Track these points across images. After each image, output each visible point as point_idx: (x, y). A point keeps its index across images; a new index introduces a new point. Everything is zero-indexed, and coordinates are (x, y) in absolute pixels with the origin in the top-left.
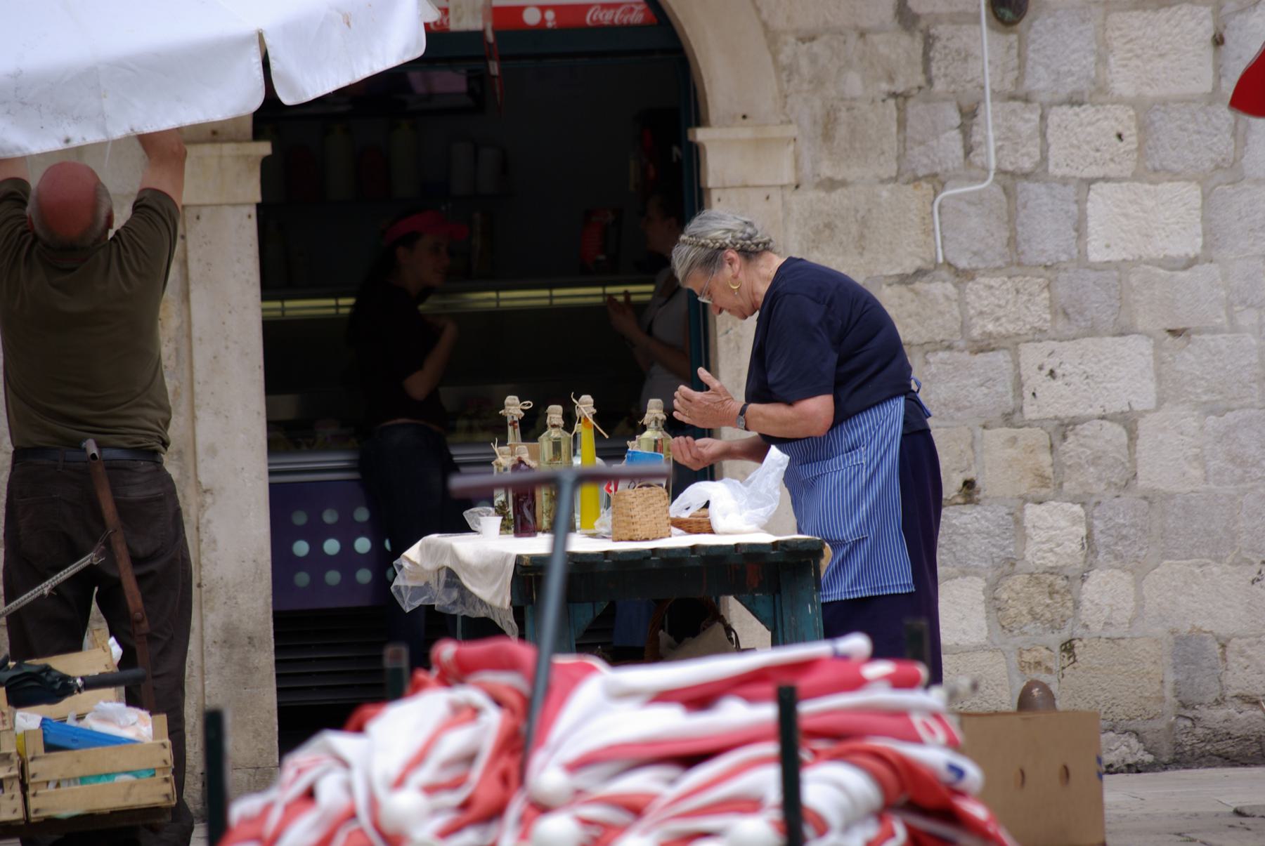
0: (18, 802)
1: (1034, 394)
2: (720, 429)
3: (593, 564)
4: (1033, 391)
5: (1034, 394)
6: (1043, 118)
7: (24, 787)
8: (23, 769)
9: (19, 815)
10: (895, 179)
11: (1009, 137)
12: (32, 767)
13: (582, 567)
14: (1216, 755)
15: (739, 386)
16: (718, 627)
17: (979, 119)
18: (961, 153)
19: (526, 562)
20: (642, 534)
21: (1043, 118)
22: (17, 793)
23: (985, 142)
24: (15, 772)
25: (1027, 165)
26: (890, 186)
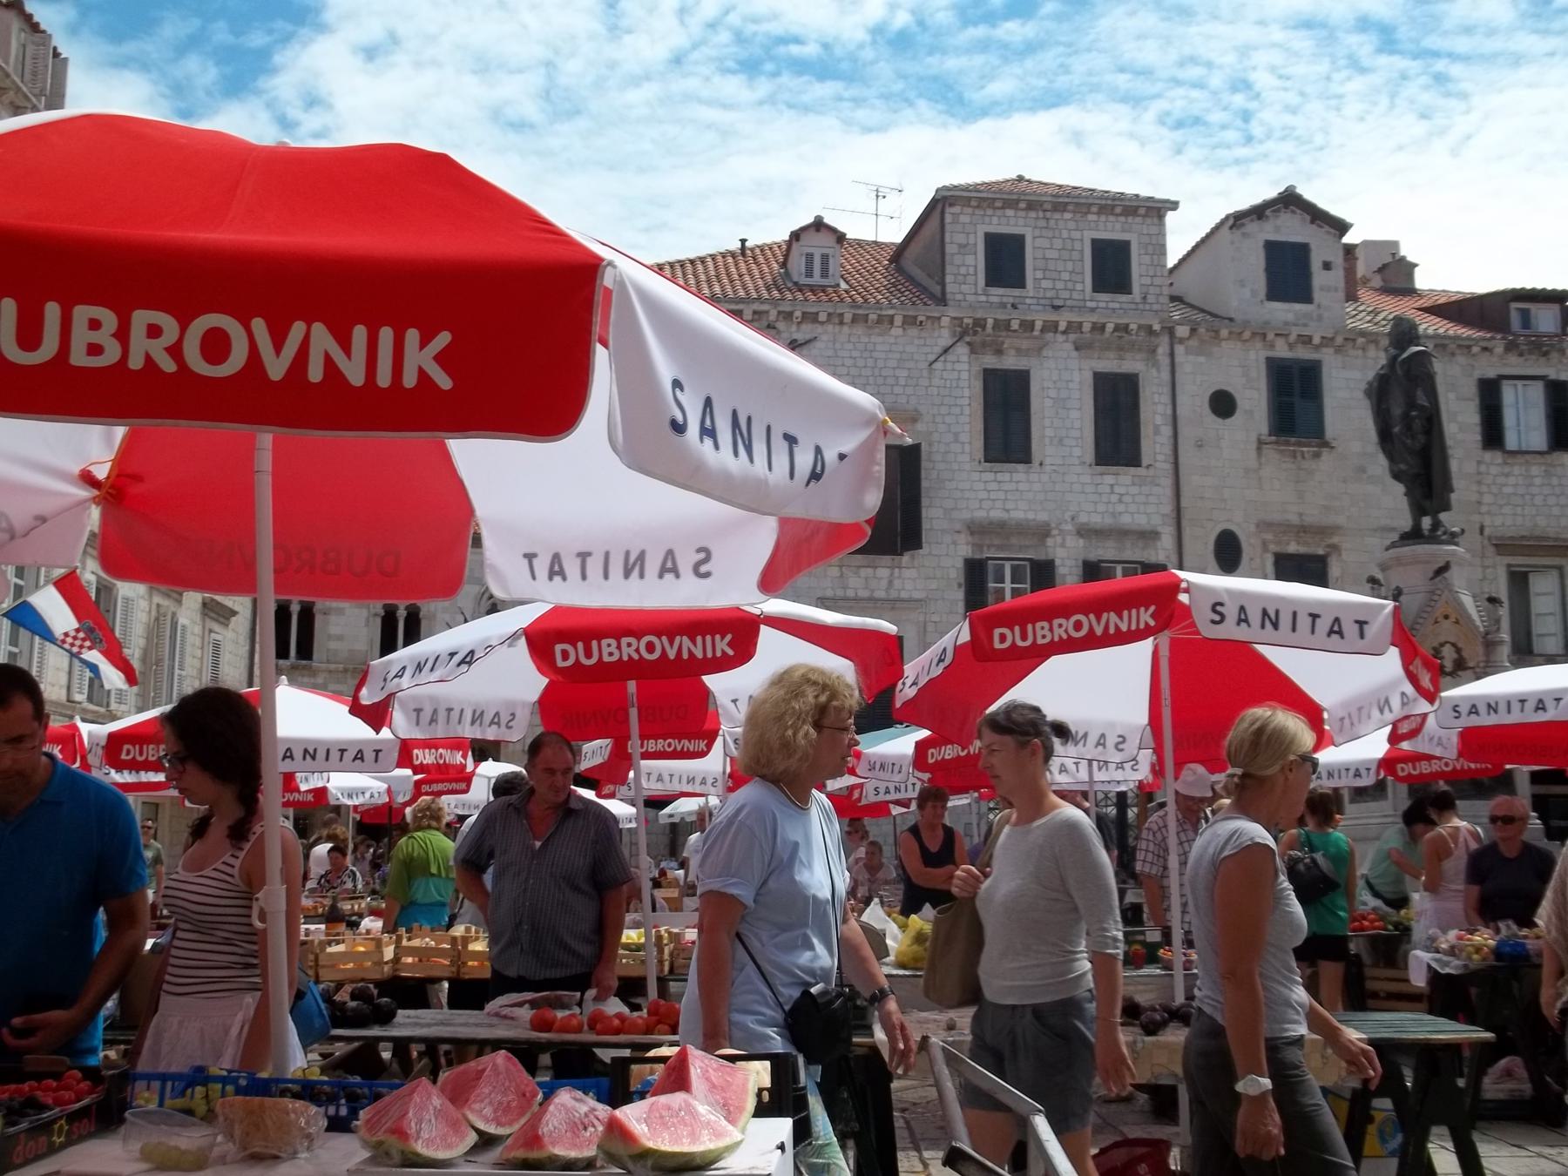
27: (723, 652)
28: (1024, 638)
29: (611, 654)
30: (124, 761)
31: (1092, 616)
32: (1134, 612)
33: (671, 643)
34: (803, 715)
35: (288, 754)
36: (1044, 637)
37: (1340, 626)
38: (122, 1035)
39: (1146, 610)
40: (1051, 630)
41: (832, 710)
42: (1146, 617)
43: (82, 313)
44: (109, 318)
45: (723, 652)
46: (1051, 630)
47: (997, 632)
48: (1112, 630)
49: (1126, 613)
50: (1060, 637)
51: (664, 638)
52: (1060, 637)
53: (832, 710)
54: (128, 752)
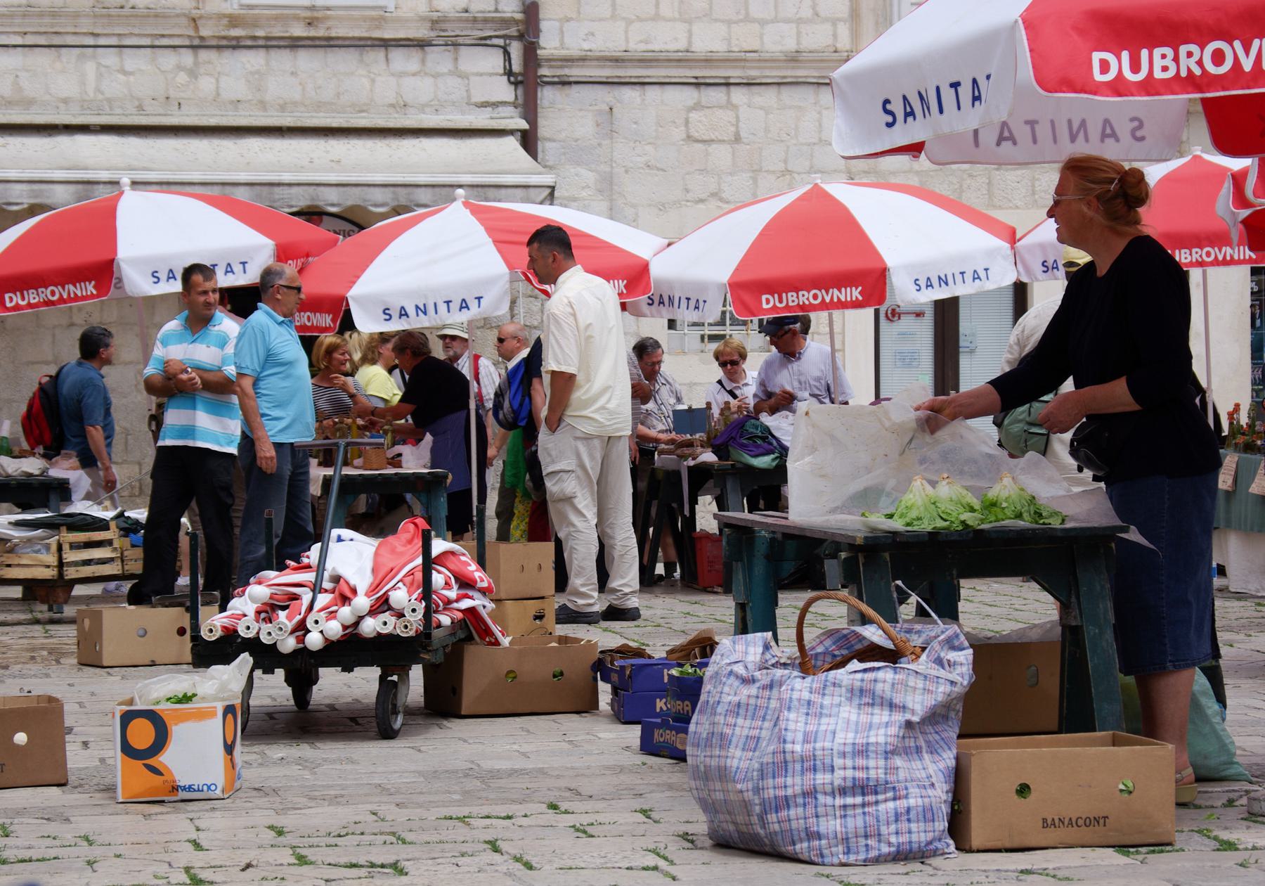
0: (120, 567)
1: (248, 866)
2: (240, 325)
3: (423, 477)
4: (254, 863)
5: (248, 866)
6: (542, 305)
7: (122, 561)
8: (122, 554)
9: (120, 572)
10: (482, 327)
11: (529, 312)
12: (126, 553)
13: (347, 483)
14: (778, 718)
15: (74, 115)
16: (405, 507)
17: (517, 304)
18: (509, 318)
19: (328, 477)
20: (375, 467)
21: (542, 305)
22: (120, 563)
23: (519, 314)
24: (119, 555)
25: (536, 323)
26: (481, 330)
27: (857, 297)
28: (781, 301)
29: (793, 301)
30: (767, 310)
31: (823, 291)
32: (848, 289)
33: (64, 289)
34: (707, 331)
35: (1055, 266)
36: (1165, 69)
37: (405, 311)
38: (201, 553)
39: (856, 289)
40: (1176, 59)
41: (546, 379)
42: (855, 293)
43: (790, 294)
44: (795, 294)
45: (857, 297)
46: (1176, 59)
47: (764, 297)
48: (1228, 258)
49: (843, 290)
50: (1197, 260)
51: (59, 287)
52: (1197, 260)
53: (546, 379)
54: (768, 301)
